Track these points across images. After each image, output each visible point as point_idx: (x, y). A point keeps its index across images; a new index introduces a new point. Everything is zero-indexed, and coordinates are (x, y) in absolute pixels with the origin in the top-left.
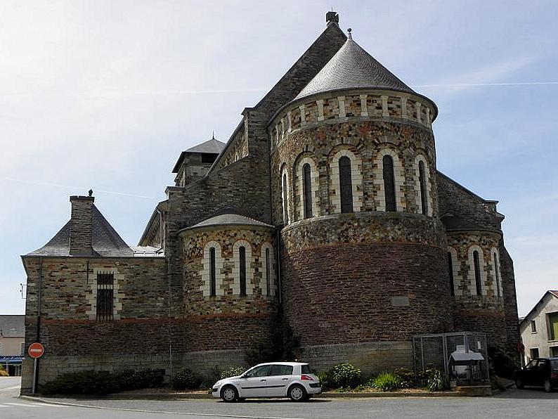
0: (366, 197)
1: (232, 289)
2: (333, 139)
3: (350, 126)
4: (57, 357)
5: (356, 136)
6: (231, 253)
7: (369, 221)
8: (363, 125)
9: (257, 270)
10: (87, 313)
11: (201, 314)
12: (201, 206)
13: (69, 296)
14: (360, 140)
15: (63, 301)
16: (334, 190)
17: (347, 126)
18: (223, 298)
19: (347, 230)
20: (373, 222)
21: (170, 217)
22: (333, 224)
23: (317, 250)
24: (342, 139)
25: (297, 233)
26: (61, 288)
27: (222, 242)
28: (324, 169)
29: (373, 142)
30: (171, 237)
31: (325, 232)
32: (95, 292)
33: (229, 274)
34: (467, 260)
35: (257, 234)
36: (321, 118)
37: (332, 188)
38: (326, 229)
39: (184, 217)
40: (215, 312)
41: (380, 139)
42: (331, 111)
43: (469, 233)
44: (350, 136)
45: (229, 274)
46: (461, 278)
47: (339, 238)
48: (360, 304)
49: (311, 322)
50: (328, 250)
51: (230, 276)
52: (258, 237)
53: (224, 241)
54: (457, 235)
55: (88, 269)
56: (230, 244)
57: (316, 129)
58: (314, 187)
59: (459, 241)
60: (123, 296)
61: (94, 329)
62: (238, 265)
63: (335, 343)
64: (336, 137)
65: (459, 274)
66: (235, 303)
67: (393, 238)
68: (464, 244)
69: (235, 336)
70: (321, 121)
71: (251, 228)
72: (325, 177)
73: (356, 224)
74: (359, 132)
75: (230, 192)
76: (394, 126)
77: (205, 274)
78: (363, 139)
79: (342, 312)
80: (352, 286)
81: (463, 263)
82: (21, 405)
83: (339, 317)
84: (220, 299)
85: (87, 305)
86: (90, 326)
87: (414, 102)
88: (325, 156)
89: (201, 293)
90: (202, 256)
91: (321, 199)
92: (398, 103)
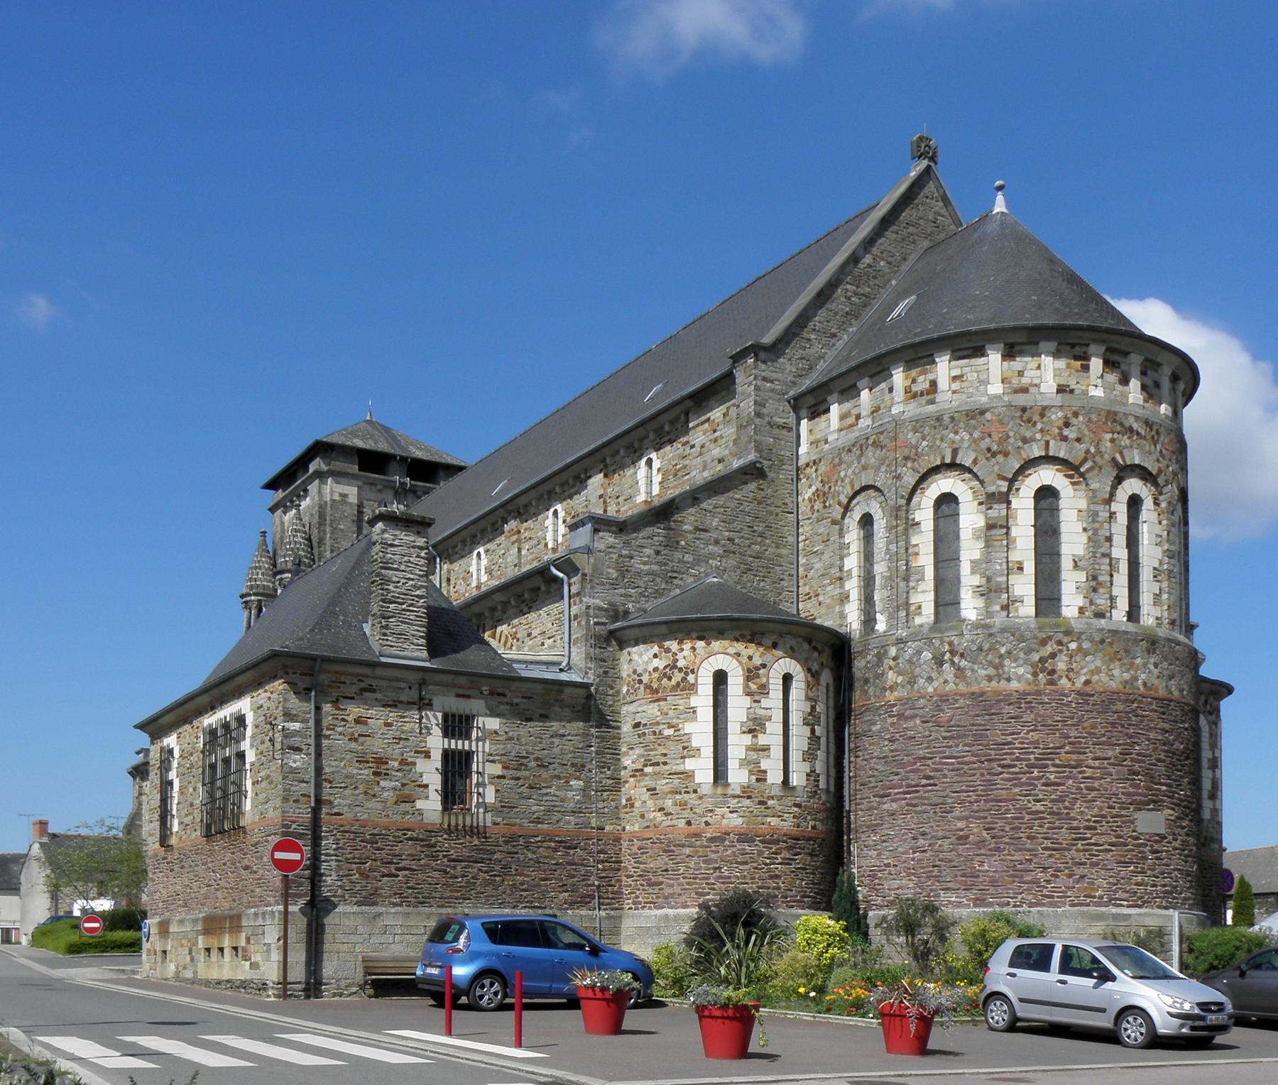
0: (1095, 584)
1: (765, 772)
2: (1025, 441)
3: (1066, 417)
4: (355, 908)
5: (1078, 440)
6: (764, 690)
7: (1102, 641)
8: (1094, 417)
10: (419, 804)
11: (689, 823)
12: (655, 567)
13: (381, 761)
14: (1087, 452)
15: (367, 772)
16: (1020, 563)
17: (1060, 414)
18: (747, 793)
19: (1053, 656)
20: (1111, 644)
21: (592, 588)
22: (1022, 639)
23: (977, 697)
24: (1047, 443)
25: (919, 652)
26: (361, 739)
27: (745, 660)
28: (998, 511)
29: (1114, 459)
30: (597, 637)
31: (1001, 656)
32: (437, 756)
33: (760, 736)
36: (996, 388)
37: (1015, 556)
38: (1003, 650)
39: (622, 591)
40: (725, 822)
41: (1125, 452)
42: (1021, 374)
44: (1065, 439)
45: (760, 736)
47: (1035, 675)
48: (1075, 824)
49: (952, 855)
50: (1005, 698)
51: (762, 740)
53: (750, 658)
55: (421, 699)
56: (764, 666)
57: (983, 413)
58: (970, 550)
60: (496, 769)
61: (434, 846)
62: (778, 715)
63: (1014, 906)
64: (1033, 440)
66: (770, 803)
67: (1145, 684)
69: (771, 877)
70: (998, 397)
71: (804, 631)
72: (997, 529)
73: (1073, 646)
74: (1086, 433)
77: (700, 731)
78: (1093, 450)
79: (1034, 838)
82: (157, 994)
83: (1029, 850)
84: (738, 792)
85: (419, 786)
86: (426, 838)
88: (1005, 479)
89: (689, 775)
90: (693, 688)
91: (989, 580)
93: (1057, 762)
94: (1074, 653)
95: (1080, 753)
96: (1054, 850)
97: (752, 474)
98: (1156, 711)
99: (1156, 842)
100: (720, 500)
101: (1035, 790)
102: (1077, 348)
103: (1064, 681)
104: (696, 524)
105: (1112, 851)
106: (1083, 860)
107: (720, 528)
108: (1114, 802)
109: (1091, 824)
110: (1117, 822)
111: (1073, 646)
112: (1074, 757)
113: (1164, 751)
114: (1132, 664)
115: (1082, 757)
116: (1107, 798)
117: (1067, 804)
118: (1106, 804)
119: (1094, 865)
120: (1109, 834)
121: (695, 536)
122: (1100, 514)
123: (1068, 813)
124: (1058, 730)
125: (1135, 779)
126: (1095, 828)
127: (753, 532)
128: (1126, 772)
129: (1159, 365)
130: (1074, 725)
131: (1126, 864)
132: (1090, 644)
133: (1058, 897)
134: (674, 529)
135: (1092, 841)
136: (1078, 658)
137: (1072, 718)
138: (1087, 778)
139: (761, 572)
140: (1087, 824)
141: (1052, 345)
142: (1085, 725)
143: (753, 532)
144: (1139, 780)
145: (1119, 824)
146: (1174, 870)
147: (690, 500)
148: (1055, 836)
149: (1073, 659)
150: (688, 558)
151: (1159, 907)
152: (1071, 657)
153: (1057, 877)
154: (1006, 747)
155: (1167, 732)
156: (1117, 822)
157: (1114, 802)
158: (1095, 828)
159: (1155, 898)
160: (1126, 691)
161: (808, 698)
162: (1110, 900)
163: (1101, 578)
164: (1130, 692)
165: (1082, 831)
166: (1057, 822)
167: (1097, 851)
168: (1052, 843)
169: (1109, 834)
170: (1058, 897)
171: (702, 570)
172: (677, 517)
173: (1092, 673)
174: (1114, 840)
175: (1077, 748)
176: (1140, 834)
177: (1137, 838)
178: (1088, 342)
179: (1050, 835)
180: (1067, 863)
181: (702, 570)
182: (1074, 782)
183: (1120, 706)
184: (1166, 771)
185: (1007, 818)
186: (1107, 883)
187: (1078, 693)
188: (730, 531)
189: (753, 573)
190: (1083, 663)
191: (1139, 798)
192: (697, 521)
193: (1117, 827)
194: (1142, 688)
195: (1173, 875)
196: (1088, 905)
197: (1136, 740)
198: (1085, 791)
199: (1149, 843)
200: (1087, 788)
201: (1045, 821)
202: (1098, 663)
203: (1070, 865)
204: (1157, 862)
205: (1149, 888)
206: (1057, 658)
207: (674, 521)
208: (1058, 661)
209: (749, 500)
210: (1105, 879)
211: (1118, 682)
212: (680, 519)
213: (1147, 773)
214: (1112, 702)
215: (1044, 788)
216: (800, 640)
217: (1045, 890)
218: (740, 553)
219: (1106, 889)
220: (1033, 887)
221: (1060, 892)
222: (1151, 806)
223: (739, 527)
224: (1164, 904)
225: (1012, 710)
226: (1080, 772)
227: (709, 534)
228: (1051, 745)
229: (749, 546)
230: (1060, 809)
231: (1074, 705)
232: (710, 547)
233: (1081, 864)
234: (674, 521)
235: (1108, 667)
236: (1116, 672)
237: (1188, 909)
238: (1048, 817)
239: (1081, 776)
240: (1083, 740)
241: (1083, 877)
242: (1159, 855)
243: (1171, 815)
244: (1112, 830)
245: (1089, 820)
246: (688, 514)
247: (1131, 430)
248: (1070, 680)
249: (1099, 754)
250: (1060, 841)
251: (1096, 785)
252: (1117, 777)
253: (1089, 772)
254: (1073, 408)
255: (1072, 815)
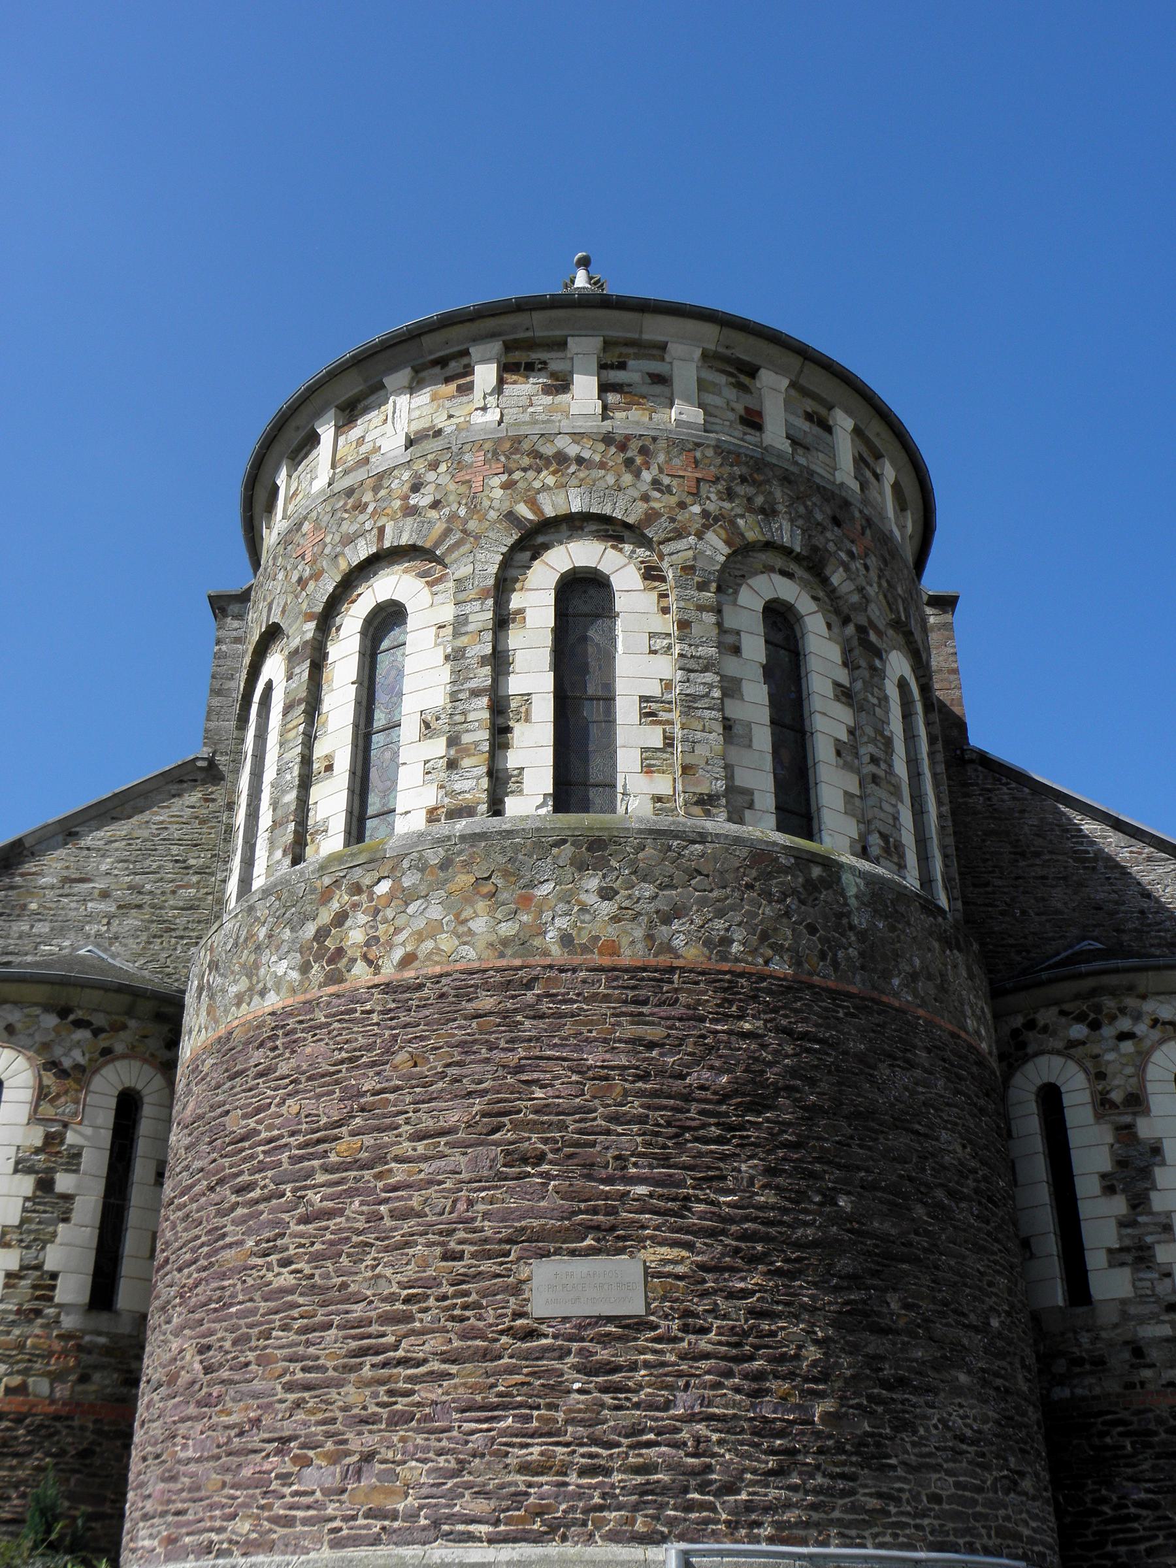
7: (445, 864)
9: (45, 1185)
20: (466, 864)
34: (1147, 1112)
35: (79, 1024)
43: (1146, 981)
46: (1119, 1205)
47: (305, 969)
48: (358, 1311)
52: (83, 1034)
54: (1078, 996)
59: (1095, 1026)
65: (1109, 1190)
67: (566, 940)
68: (1123, 1036)
74: (452, 487)
75: (105, 895)
76: (623, 447)
80: (330, 1214)
81: (1126, 1133)
87: (752, 371)
92: (655, 367)
93: (333, 1158)
94: (383, 901)
95: (380, 1130)
96: (307, 1387)
97: (195, 781)
98: (606, 998)
99: (604, 1340)
100: (121, 829)
101: (282, 1235)
102: (453, 364)
103: (360, 968)
104: (65, 873)
105: (448, 1375)
106: (373, 1409)
107: (116, 872)
108: (460, 1242)
109: (399, 1306)
110: (466, 1294)
111: (384, 887)
112: (368, 1140)
113: (640, 1094)
114: (526, 900)
115: (386, 1138)
116: (440, 1233)
117: (344, 1261)
118: (438, 1250)
119: (399, 1420)
120: (445, 1330)
121: (60, 891)
122: (471, 618)
123: (344, 1285)
124: (337, 1082)
125: (529, 1175)
126: (408, 1318)
127: (186, 868)
128: (500, 1157)
129: (663, 347)
130: (374, 1064)
131: (490, 1411)
132: (419, 875)
133: (306, 1522)
134: (21, 887)
135: (400, 1353)
136: (389, 913)
137: (370, 1048)
138: (395, 1189)
139: (193, 930)
140: (387, 1307)
141: (403, 376)
142: (401, 1057)
143: (186, 868)
144: (540, 1175)
145: (474, 1297)
146: (691, 1418)
147: (60, 838)
148: (311, 1350)
149: (379, 918)
150: (42, 928)
151: (614, 1537)
152: (377, 911)
153: (308, 1463)
154: (246, 1144)
155: (651, 1046)
156: (466, 1294)
157: (460, 1242)
158: (408, 1318)
159: (600, 1508)
160: (503, 963)
161: (35, 1118)
162: (436, 1524)
163: (466, 739)
164: (517, 962)
165: (375, 1328)
166: (321, 1311)
167: (410, 1379)
168: (303, 1370)
169: (445, 1330)
170: (306, 1522)
171: (67, 943)
172: (30, 867)
173: (420, 937)
174: (456, 1343)
175: (377, 1117)
176: (541, 1321)
177: (530, 1334)
178: (464, 347)
179: (301, 1350)
180: (333, 1421)
181: (67, 943)
182: (362, 1203)
183: (486, 1002)
184: (647, 1144)
185: (231, 1316)
186: (430, 1471)
187: (388, 988)
188: (136, 874)
189: (178, 933)
190: (401, 921)
191: (535, 1223)
192: (67, 868)
193: (465, 1307)
194: (555, 950)
195: (684, 1435)
196: (376, 1541)
197: (535, 1076)
198: (388, 1222)
199: (575, 1346)
200: (393, 1215)
201: (295, 1313)
202: (436, 912)
203: (338, 1426)
204: (607, 1398)
205: (573, 1478)
206: (349, 923)
207: (22, 875)
208: (350, 928)
209: (184, 820)
210: (424, 1461)
211: (481, 944)
212: (34, 869)
213: (570, 1156)
214: (465, 993)
215: (302, 1227)
216: (37, 1011)
217: (278, 1503)
218: (153, 906)
219: (425, 1491)
220: (253, 1496)
221: (309, 1507)
222: (589, 1242)
223: (155, 865)
224: (639, 1526)
225: (258, 1056)
226: (379, 1176)
227: (92, 885)
228: (324, 1120)
229: (174, 892)
230: (327, 1276)
231: (375, 1018)
232: (90, 905)
233: (364, 1421)
234: (22, 875)
235: (457, 916)
236: (479, 925)
237: (771, 1540)
238: (301, 1300)
239: (380, 1185)
240: (391, 1096)
241: (368, 1457)
242: (616, 1377)
243: (681, 1261)
244: (453, 1318)
245: (391, 1298)
246: (51, 860)
247: (561, 458)
248: (370, 962)
249: (428, 1123)
250: (321, 1362)
251: (415, 1203)
252: (473, 1175)
253: (400, 1171)
254: (430, 457)
255: (353, 1288)
